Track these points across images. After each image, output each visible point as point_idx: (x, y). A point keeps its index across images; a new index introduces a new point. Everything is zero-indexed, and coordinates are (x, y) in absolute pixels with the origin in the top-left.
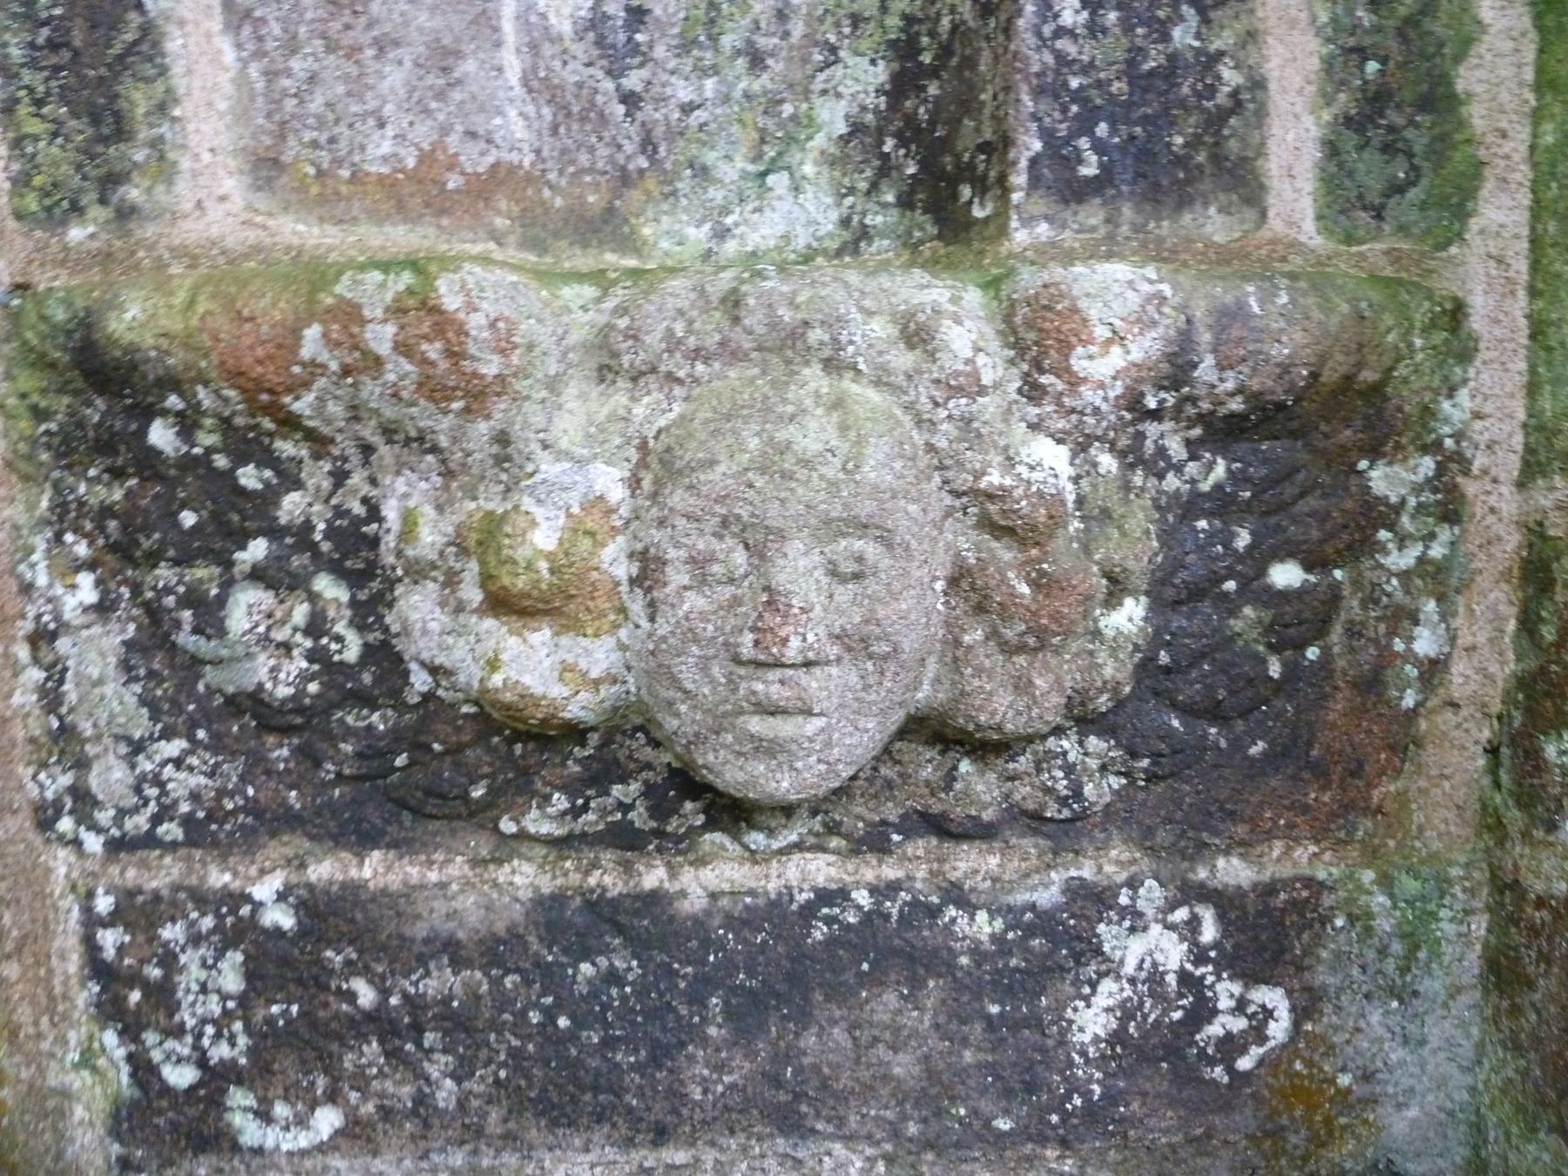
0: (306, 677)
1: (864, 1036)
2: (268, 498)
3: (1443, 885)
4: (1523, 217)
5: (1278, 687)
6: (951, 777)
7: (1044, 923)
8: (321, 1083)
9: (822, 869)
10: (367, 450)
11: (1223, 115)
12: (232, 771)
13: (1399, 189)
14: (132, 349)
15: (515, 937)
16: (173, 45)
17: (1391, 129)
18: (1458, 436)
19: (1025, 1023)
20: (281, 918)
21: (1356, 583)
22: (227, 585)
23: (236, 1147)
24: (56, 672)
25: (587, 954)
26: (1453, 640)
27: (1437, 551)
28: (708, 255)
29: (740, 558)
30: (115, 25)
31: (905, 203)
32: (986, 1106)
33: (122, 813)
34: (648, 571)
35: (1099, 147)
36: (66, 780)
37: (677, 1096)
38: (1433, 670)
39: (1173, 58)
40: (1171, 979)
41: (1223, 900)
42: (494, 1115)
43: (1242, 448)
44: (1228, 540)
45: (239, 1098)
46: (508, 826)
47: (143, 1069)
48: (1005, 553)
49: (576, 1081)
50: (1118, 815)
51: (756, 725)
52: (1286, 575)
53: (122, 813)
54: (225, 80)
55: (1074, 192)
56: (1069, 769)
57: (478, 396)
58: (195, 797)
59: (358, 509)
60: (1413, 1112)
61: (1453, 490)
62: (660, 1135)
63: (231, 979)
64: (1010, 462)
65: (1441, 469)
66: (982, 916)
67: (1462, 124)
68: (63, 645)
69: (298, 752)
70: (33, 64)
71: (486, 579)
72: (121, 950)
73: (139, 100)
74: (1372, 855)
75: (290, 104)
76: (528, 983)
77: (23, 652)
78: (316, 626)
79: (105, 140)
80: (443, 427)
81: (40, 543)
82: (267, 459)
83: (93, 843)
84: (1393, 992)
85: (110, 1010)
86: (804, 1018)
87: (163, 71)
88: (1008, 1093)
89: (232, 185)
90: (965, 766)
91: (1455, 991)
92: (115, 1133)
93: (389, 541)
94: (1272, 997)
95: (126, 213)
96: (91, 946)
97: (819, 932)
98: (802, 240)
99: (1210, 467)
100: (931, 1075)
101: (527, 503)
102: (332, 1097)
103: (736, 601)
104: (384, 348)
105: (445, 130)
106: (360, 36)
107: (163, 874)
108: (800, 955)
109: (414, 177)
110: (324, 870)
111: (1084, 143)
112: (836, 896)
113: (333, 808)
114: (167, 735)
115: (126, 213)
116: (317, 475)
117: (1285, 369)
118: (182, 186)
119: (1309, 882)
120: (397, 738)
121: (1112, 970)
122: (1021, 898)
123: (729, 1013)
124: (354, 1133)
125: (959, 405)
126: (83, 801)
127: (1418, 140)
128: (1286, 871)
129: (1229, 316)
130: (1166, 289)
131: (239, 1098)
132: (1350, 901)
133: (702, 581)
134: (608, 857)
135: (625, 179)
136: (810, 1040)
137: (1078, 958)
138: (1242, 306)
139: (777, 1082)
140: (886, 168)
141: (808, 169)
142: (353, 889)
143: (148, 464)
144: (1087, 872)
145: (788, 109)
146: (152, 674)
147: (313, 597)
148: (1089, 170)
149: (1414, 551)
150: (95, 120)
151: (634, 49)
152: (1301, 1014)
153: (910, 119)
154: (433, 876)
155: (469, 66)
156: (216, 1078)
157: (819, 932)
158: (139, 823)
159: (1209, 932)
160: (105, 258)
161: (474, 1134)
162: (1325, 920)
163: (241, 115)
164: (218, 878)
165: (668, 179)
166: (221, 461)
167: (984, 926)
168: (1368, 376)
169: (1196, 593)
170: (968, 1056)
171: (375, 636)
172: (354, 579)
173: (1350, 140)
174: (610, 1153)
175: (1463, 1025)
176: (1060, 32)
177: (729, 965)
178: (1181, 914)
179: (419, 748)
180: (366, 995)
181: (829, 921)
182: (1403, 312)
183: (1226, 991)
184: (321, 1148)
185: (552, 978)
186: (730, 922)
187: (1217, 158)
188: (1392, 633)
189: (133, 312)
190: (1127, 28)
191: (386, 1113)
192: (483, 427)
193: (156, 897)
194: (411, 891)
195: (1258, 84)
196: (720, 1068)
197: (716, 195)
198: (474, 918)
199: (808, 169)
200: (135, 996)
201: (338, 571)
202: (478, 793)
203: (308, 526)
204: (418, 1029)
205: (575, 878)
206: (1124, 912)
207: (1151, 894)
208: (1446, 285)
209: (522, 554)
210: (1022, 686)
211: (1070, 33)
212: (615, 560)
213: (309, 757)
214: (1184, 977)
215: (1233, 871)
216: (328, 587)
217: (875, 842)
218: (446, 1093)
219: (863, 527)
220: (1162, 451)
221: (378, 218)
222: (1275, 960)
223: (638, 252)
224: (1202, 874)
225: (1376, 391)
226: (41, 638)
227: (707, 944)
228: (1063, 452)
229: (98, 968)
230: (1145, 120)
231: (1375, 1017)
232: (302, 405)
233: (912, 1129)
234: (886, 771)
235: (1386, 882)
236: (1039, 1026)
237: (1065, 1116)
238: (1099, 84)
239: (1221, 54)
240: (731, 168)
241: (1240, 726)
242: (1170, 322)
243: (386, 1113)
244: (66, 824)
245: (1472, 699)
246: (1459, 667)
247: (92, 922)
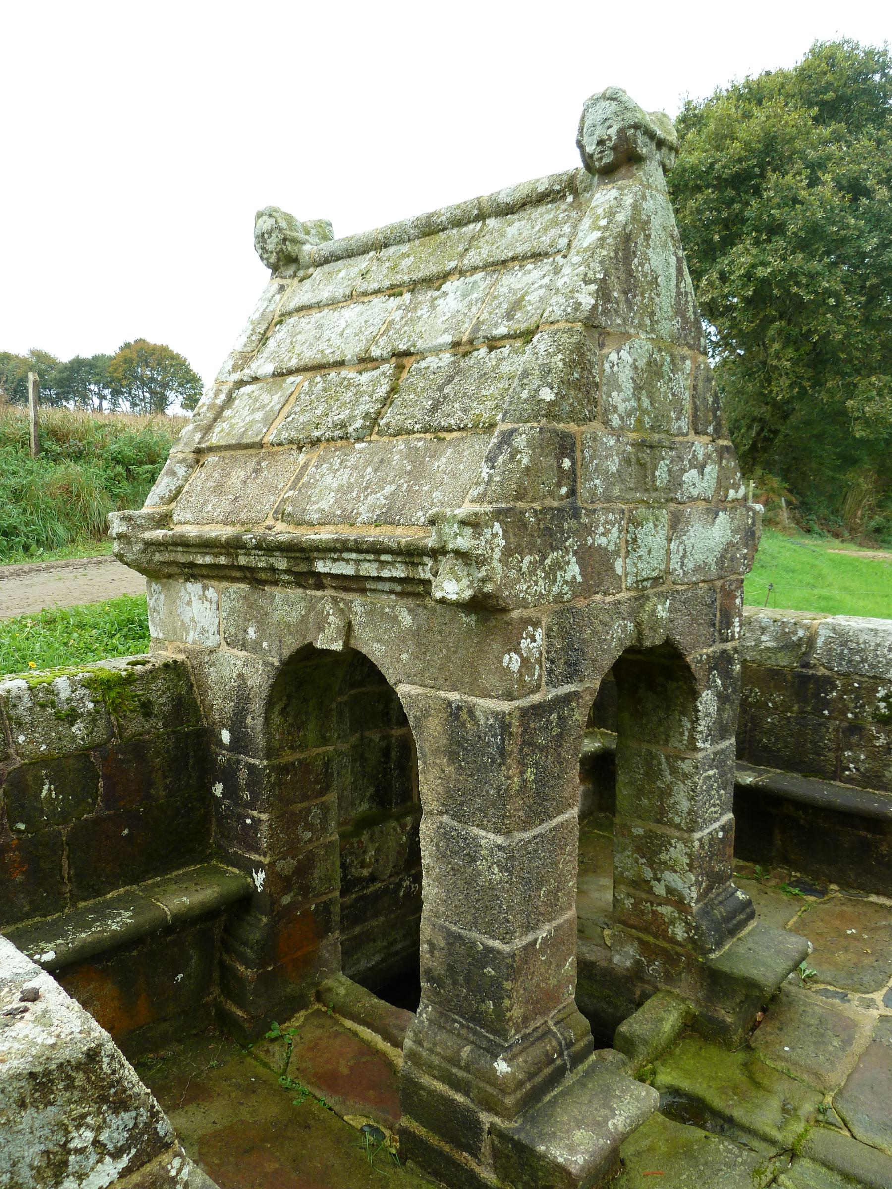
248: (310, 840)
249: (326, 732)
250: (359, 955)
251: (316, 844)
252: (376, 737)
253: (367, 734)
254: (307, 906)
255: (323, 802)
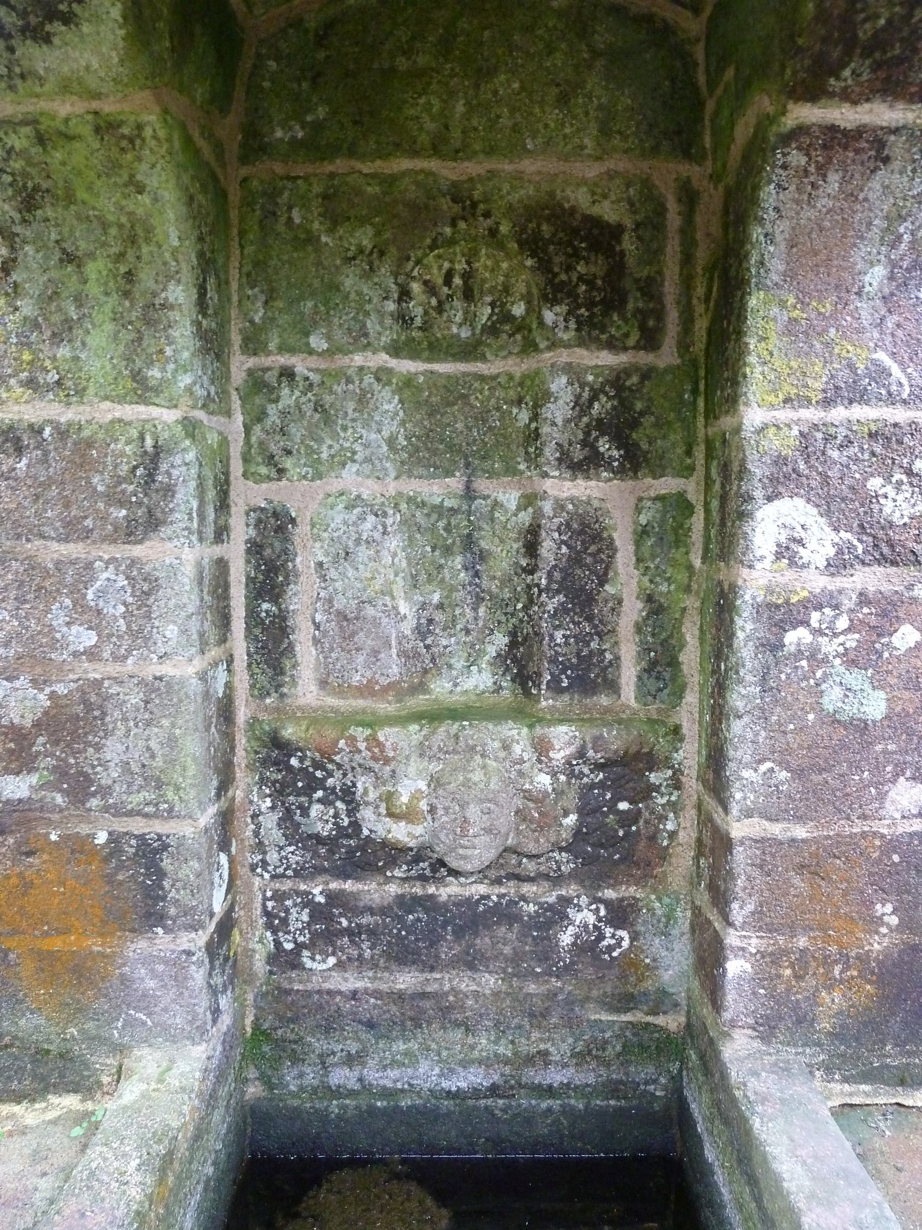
0: (332, 830)
1: (495, 940)
2: (325, 779)
3: (678, 901)
4: (697, 701)
5: (623, 839)
6: (520, 863)
7: (550, 907)
8: (330, 949)
9: (482, 889)
10: (353, 768)
11: (606, 668)
12: (308, 856)
13: (660, 690)
14: (289, 740)
15: (390, 907)
16: (298, 648)
17: (658, 672)
18: (679, 764)
19: (545, 938)
20: (321, 899)
21: (647, 808)
22: (310, 803)
23: (304, 968)
24: (259, 826)
25: (411, 912)
26: (679, 825)
27: (673, 798)
28: (451, 692)
29: (457, 808)
30: (281, 642)
31: (513, 680)
32: (532, 963)
33: (276, 867)
34: (432, 810)
35: (568, 677)
36: (260, 857)
37: (437, 957)
38: (673, 835)
39: (591, 652)
40: (591, 927)
41: (607, 903)
42: (382, 961)
43: (608, 769)
44: (604, 796)
45: (306, 953)
46: (389, 874)
47: (277, 943)
48: (531, 805)
49: (407, 951)
50: (574, 876)
51: (461, 851)
52: (623, 806)
53: (276, 867)
54: (313, 660)
55: (560, 691)
56: (556, 862)
57: (387, 761)
58: (297, 863)
59: (350, 784)
60: (671, 972)
61: (678, 780)
62: (432, 969)
63: (305, 918)
64: (531, 783)
65: (674, 774)
66: (531, 905)
67: (681, 671)
68: (261, 818)
69: (328, 851)
70: (257, 653)
71: (387, 809)
72: (273, 908)
73: (287, 664)
74: (654, 890)
75: (331, 666)
76: (393, 920)
77: (249, 820)
78: (336, 816)
79: (277, 675)
80: (376, 766)
81: (255, 789)
82: (323, 768)
83: (267, 876)
84: (662, 933)
85: (269, 926)
86: (476, 934)
87: (295, 656)
88: (540, 960)
89: (314, 688)
90: (524, 860)
91: (683, 934)
92: (268, 963)
93: (359, 794)
94: (623, 933)
95: (282, 696)
96: (264, 906)
97: (481, 908)
98: (482, 687)
99: (597, 776)
100: (516, 953)
101: (400, 789)
102: (333, 954)
103: (456, 819)
104: (363, 748)
105: (375, 673)
106: (351, 647)
107: (286, 886)
108: (475, 914)
109: (366, 686)
110: (334, 885)
111: (563, 676)
112: (487, 897)
113: (337, 867)
114: (290, 845)
115: (282, 696)
116: (338, 774)
117: (616, 751)
118: (299, 688)
119: (634, 898)
120: (358, 848)
121: (572, 923)
122: (543, 900)
123: (454, 931)
124: (340, 965)
125: (517, 767)
126: (264, 864)
127: (667, 676)
128: (627, 895)
129: (597, 740)
130: (577, 734)
131: (306, 953)
132: (647, 904)
133: (447, 813)
134: (418, 883)
135: (426, 671)
136: (478, 941)
137: (562, 919)
138: (602, 735)
139: (468, 954)
140: (507, 669)
141: (484, 666)
142: (342, 891)
143: (290, 768)
144: (564, 893)
145: (477, 647)
146: (286, 827)
147: (335, 808)
148: (565, 684)
149: (666, 798)
150: (275, 670)
151: (429, 631)
152: (632, 939)
153: (515, 656)
154: (366, 888)
155: (382, 655)
156: (299, 947)
157: (481, 908)
158: (280, 870)
159: (603, 912)
160: (277, 710)
161: (376, 966)
162: (640, 910)
163: (316, 669)
164: (303, 887)
165: (439, 669)
166: (311, 770)
167: (532, 908)
168: (645, 750)
169: (595, 811)
170: (527, 948)
171: (353, 819)
172: (348, 803)
173: (646, 676)
174: (417, 974)
175: (685, 945)
176: (556, 645)
177: (454, 917)
178: (594, 907)
179: (364, 851)
180: (345, 923)
181: (484, 905)
182: (656, 732)
183: (608, 931)
184: (329, 969)
185: (401, 920)
186: (454, 904)
187: (605, 680)
188: (659, 823)
189: (290, 731)
190: (577, 643)
191: (349, 959)
192: (388, 768)
193: (284, 892)
194: (359, 892)
195: (617, 658)
196: (451, 949)
197: (454, 673)
198: (378, 901)
199: (484, 666)
200: (277, 922)
201: (343, 800)
202: (380, 864)
203: (335, 788)
204: (360, 934)
205: (408, 890)
206: (575, 905)
207: (584, 900)
208: (673, 720)
209: (398, 803)
210: (537, 841)
211: (559, 645)
212: (423, 805)
213: (331, 852)
214: (595, 926)
215: (610, 894)
216: (340, 805)
217: (498, 881)
218: (367, 953)
219: (490, 801)
220: (581, 772)
221: (356, 698)
222: (624, 922)
223: (429, 693)
224: (600, 894)
225: (650, 754)
226: (255, 816)
227: (447, 911)
228: (549, 777)
229: (267, 913)
230: (582, 670)
231: (657, 941)
232: (337, 758)
233: (510, 970)
234: (501, 861)
235: (659, 899)
236: (549, 940)
237: (558, 968)
238: (569, 660)
239: (605, 650)
240: (459, 663)
241: (611, 850)
242: (578, 742)
243: (349, 959)
244: (259, 870)
245: (686, 843)
246: (681, 834)
247: (265, 899)
248: (92, 654)
249: (150, 364)
250: (414, 1045)
251: (113, 669)
252: (510, 498)
253: (482, 485)
254: (84, 829)
255: (133, 562)
